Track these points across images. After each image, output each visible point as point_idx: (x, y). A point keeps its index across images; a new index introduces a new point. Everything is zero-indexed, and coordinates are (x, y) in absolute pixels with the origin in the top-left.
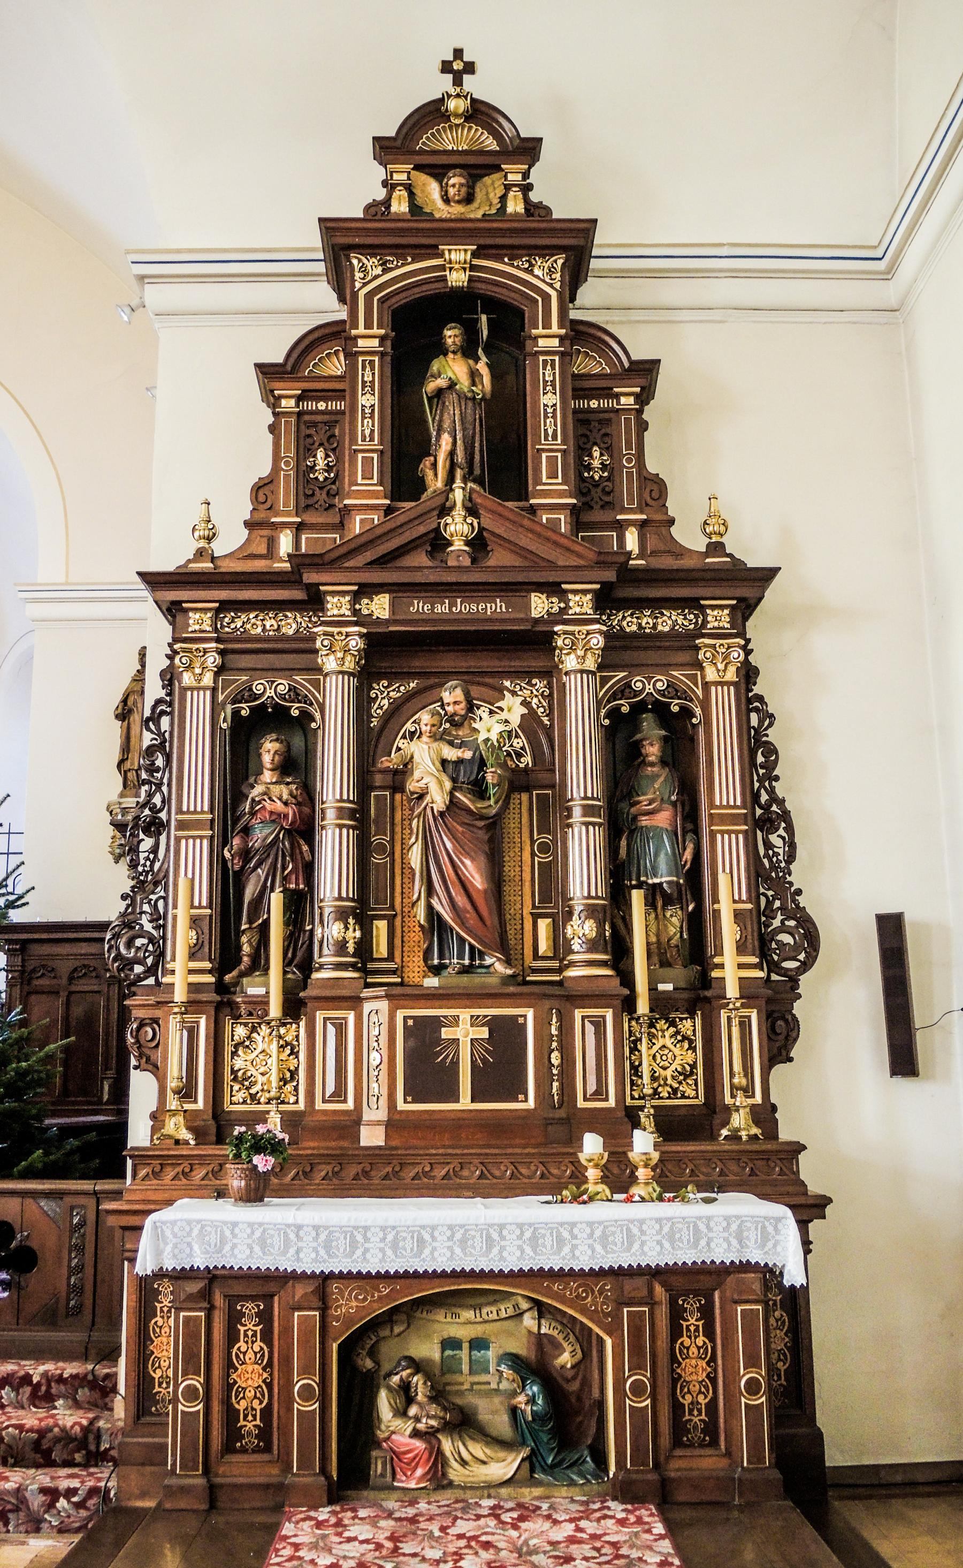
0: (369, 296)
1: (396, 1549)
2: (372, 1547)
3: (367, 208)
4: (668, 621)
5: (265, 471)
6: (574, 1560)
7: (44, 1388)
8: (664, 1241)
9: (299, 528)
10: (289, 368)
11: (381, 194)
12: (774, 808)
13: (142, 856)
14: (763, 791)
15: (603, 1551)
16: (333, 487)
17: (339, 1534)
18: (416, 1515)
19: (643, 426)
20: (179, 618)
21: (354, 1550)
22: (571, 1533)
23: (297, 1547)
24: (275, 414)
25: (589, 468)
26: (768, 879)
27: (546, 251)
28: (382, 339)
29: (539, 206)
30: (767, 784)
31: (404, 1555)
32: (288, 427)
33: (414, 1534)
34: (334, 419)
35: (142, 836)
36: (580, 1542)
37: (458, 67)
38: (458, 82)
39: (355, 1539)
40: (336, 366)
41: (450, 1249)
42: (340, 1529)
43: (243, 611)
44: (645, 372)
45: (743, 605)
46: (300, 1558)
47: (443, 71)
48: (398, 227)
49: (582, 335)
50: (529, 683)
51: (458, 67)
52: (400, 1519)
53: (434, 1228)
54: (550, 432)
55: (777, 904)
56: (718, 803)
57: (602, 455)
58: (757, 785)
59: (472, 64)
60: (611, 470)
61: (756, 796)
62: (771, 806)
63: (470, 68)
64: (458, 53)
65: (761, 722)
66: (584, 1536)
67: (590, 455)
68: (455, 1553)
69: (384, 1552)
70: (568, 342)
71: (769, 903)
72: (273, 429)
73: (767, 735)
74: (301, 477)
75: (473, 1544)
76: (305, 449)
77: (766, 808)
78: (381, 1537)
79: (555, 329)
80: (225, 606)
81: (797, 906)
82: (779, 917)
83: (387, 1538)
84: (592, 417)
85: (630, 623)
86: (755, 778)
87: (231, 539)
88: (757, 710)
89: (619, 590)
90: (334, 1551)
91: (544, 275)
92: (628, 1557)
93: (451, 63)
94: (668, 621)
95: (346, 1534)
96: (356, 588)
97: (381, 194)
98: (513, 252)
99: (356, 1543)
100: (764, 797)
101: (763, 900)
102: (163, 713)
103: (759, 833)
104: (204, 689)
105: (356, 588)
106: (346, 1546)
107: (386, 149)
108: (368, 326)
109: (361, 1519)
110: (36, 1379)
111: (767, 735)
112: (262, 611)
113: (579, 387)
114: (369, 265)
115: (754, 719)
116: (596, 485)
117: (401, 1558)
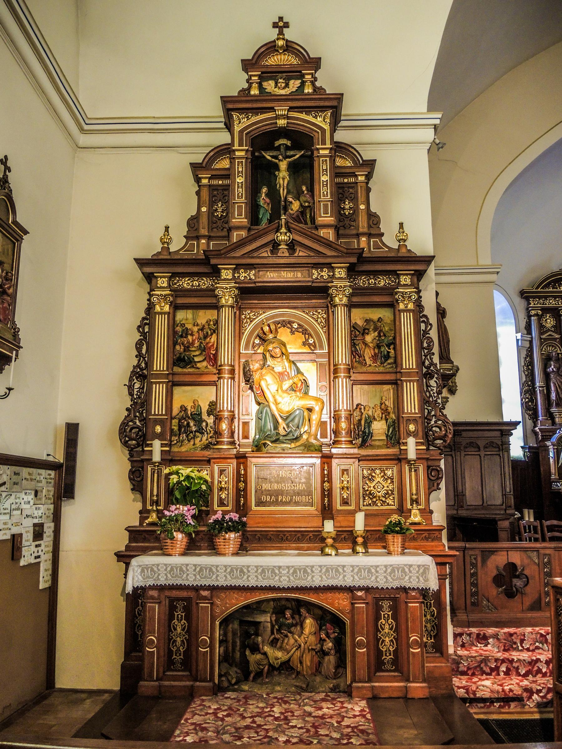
0: (241, 132)
1: (317, 732)
2: (235, 701)
3: (239, 92)
4: (382, 282)
5: (194, 213)
6: (323, 708)
8: (408, 572)
9: (209, 238)
10: (204, 165)
11: (246, 86)
12: (432, 368)
13: (136, 390)
14: (427, 361)
15: (336, 705)
16: (225, 219)
17: (287, 724)
18: (323, 715)
19: (368, 190)
20: (154, 281)
21: (295, 733)
22: (323, 697)
23: (267, 730)
24: (199, 186)
25: (344, 209)
26: (428, 402)
27: (323, 109)
28: (247, 151)
29: (321, 88)
30: (428, 357)
31: (250, 704)
32: (205, 193)
33: (325, 724)
34: (226, 188)
35: (135, 381)
36: (327, 701)
37: (281, 25)
38: (281, 33)
39: (295, 726)
40: (225, 164)
41: (321, 576)
42: (287, 722)
43: (183, 277)
44: (371, 164)
45: (417, 273)
46: (204, 705)
47: (274, 27)
48: (256, 99)
49: (340, 148)
50: (316, 311)
51: (281, 25)
52: (314, 717)
53: (313, 567)
54: (325, 193)
55: (433, 413)
56: (404, 367)
57: (349, 203)
58: (423, 357)
59: (287, 23)
60: (356, 210)
61: (423, 363)
62: (430, 367)
63: (287, 25)
64: (281, 19)
65: (426, 327)
66: (329, 698)
67: (344, 203)
68: (272, 705)
69: (241, 703)
70: (333, 152)
71: (429, 413)
72: (198, 193)
73: (429, 334)
74: (211, 214)
75: (355, 730)
76: (212, 203)
77: (428, 368)
78: (309, 726)
79: (328, 145)
80: (174, 275)
81: (442, 414)
82: (434, 420)
83: (311, 726)
84: (345, 185)
85: (362, 282)
86: (423, 354)
87: (177, 244)
88: (423, 321)
89: (358, 265)
90: (286, 733)
91: (322, 121)
92: (347, 708)
93: (277, 23)
94: (382, 282)
95: (291, 724)
96: (235, 266)
97: (246, 86)
98: (307, 110)
99: (297, 729)
100: (427, 363)
101: (426, 411)
102: (146, 324)
103: (425, 380)
104: (165, 313)
105: (235, 266)
106: (292, 730)
107: (247, 65)
108: (241, 144)
109: (297, 716)
111: (429, 334)
112: (192, 277)
113: (337, 173)
114: (241, 117)
115: (423, 326)
116: (347, 217)
117: (320, 737)
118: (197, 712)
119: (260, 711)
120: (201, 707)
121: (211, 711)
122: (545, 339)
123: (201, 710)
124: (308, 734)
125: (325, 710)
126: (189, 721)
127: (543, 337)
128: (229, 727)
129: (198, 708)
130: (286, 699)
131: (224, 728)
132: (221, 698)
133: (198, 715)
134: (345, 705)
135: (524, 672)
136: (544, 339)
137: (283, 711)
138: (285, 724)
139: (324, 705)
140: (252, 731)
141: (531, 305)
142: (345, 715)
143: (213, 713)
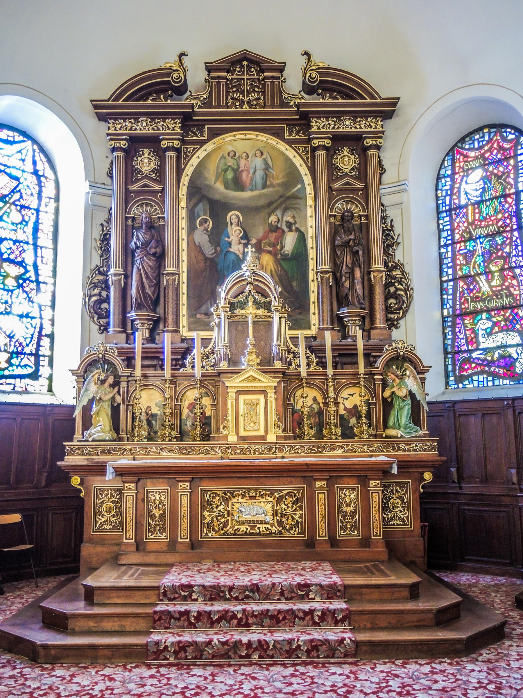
2: (202, 679)
7: (244, 620)
15: (306, 680)
18: (294, 691)
36: (296, 676)
68: (240, 682)
69: (208, 681)
92: (317, 683)
106: (191, 678)
110: (239, 616)
118: (165, 692)
119: (229, 688)
120: (168, 686)
121: (178, 690)
122: (339, 191)
123: (168, 689)
124: (205, 682)
125: (295, 685)
126: (100, 673)
127: (336, 186)
128: (135, 677)
129: (165, 687)
130: (253, 675)
131: (130, 678)
132: (187, 675)
133: (165, 694)
134: (315, 680)
135: (341, 616)
136: (337, 190)
137: (253, 688)
138: (187, 673)
139: (294, 680)
140: (155, 679)
141: (313, 130)
142: (316, 691)
143: (180, 692)
